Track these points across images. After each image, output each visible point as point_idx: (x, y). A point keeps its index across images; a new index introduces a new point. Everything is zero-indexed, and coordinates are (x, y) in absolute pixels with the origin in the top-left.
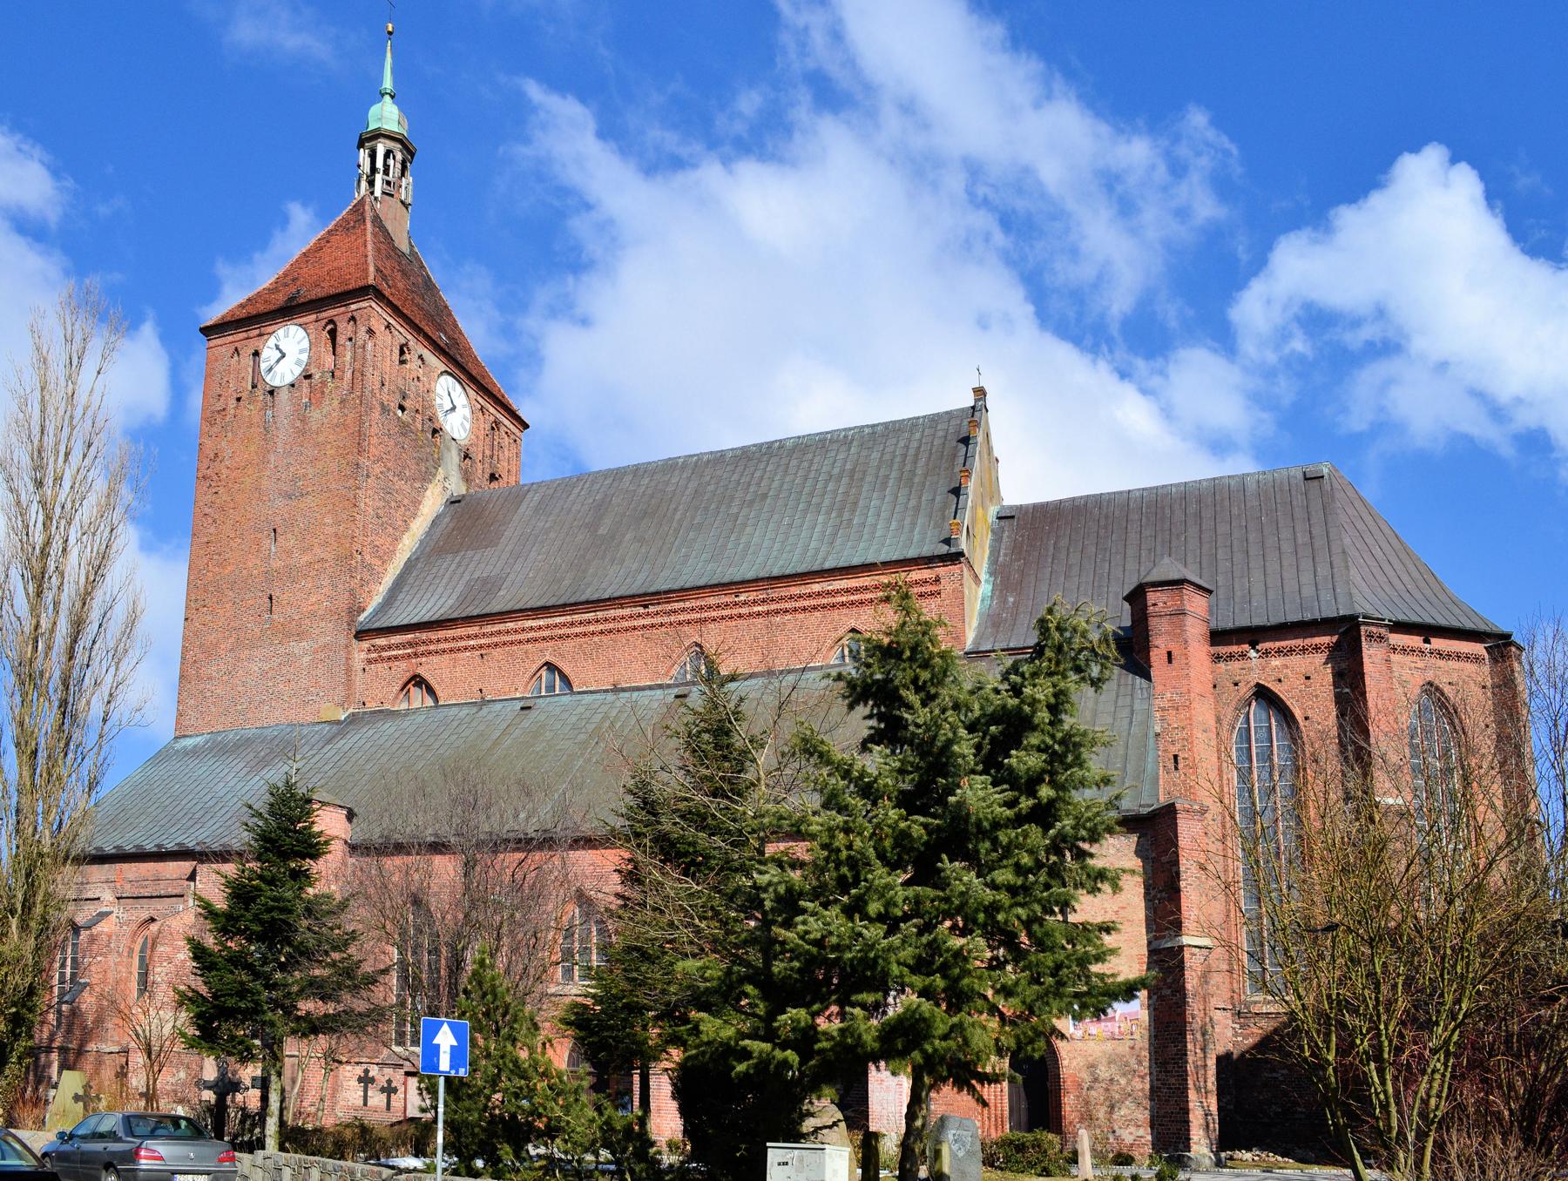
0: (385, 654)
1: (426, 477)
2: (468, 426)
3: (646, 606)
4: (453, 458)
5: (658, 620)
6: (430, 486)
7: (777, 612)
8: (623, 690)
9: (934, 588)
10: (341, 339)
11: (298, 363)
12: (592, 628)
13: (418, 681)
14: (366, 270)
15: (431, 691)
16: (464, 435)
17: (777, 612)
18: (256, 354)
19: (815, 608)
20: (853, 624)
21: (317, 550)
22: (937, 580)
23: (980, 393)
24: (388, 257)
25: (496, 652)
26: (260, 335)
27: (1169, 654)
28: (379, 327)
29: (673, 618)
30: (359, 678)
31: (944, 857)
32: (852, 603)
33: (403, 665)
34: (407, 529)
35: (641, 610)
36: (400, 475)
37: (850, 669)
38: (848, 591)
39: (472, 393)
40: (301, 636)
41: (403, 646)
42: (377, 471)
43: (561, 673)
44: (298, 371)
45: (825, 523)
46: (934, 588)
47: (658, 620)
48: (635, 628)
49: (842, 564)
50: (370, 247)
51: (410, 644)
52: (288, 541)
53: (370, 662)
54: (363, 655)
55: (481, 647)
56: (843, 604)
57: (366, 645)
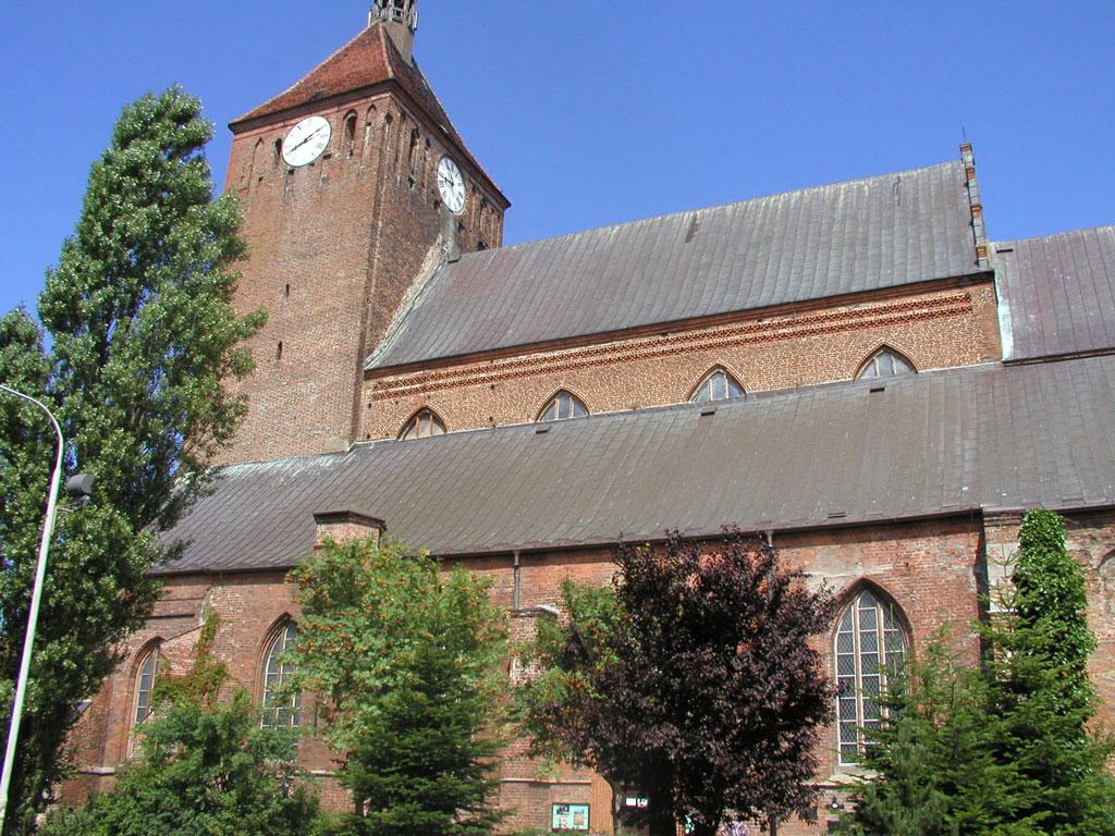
0: (391, 390)
1: (428, 240)
2: (462, 201)
3: (664, 335)
4: (452, 226)
5: (678, 346)
7: (803, 334)
8: (643, 412)
9: (965, 305)
10: (361, 123)
11: (319, 146)
12: (608, 356)
13: (424, 413)
14: (386, 71)
15: (438, 421)
16: (459, 209)
17: (803, 334)
18: (279, 144)
19: (843, 328)
20: (883, 340)
21: (329, 301)
22: (968, 298)
24: (399, 65)
26: (284, 126)
30: (364, 414)
32: (881, 322)
33: (411, 399)
34: (411, 283)
35: (661, 338)
36: (406, 237)
37: (232, 386)
38: (876, 311)
40: (309, 376)
42: (389, 232)
43: (575, 398)
44: (319, 152)
45: (839, 257)
46: (965, 305)
47: (678, 346)
48: (654, 354)
49: (868, 287)
50: (385, 55)
51: (419, 380)
53: (375, 397)
54: (369, 392)
55: (492, 378)
56: (872, 323)
57: (372, 383)
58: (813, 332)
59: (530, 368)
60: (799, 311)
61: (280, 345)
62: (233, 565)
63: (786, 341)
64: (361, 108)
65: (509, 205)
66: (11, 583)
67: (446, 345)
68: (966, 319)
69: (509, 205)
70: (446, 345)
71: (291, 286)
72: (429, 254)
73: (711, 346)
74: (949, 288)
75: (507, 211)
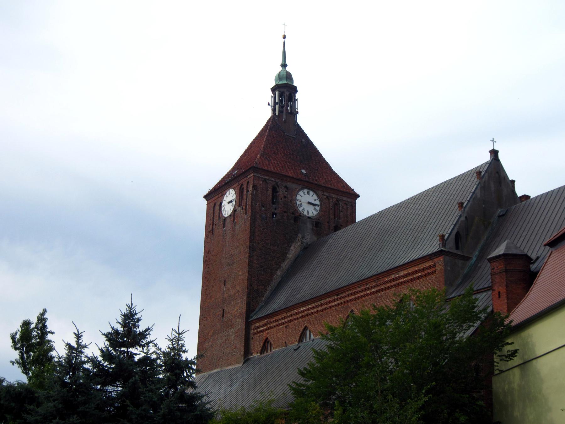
4: (309, 226)
7: (364, 296)
9: (433, 270)
22: (434, 266)
27: (499, 293)
31: (60, 406)
39: (320, 193)
40: (232, 326)
46: (433, 270)
51: (266, 325)
58: (382, 290)
59: (294, 317)
60: (289, 311)
63: (373, 296)
64: (244, 181)
65: (358, 196)
68: (433, 277)
69: (358, 196)
71: (227, 280)
72: (292, 248)
73: (350, 301)
74: (329, 297)
75: (358, 201)
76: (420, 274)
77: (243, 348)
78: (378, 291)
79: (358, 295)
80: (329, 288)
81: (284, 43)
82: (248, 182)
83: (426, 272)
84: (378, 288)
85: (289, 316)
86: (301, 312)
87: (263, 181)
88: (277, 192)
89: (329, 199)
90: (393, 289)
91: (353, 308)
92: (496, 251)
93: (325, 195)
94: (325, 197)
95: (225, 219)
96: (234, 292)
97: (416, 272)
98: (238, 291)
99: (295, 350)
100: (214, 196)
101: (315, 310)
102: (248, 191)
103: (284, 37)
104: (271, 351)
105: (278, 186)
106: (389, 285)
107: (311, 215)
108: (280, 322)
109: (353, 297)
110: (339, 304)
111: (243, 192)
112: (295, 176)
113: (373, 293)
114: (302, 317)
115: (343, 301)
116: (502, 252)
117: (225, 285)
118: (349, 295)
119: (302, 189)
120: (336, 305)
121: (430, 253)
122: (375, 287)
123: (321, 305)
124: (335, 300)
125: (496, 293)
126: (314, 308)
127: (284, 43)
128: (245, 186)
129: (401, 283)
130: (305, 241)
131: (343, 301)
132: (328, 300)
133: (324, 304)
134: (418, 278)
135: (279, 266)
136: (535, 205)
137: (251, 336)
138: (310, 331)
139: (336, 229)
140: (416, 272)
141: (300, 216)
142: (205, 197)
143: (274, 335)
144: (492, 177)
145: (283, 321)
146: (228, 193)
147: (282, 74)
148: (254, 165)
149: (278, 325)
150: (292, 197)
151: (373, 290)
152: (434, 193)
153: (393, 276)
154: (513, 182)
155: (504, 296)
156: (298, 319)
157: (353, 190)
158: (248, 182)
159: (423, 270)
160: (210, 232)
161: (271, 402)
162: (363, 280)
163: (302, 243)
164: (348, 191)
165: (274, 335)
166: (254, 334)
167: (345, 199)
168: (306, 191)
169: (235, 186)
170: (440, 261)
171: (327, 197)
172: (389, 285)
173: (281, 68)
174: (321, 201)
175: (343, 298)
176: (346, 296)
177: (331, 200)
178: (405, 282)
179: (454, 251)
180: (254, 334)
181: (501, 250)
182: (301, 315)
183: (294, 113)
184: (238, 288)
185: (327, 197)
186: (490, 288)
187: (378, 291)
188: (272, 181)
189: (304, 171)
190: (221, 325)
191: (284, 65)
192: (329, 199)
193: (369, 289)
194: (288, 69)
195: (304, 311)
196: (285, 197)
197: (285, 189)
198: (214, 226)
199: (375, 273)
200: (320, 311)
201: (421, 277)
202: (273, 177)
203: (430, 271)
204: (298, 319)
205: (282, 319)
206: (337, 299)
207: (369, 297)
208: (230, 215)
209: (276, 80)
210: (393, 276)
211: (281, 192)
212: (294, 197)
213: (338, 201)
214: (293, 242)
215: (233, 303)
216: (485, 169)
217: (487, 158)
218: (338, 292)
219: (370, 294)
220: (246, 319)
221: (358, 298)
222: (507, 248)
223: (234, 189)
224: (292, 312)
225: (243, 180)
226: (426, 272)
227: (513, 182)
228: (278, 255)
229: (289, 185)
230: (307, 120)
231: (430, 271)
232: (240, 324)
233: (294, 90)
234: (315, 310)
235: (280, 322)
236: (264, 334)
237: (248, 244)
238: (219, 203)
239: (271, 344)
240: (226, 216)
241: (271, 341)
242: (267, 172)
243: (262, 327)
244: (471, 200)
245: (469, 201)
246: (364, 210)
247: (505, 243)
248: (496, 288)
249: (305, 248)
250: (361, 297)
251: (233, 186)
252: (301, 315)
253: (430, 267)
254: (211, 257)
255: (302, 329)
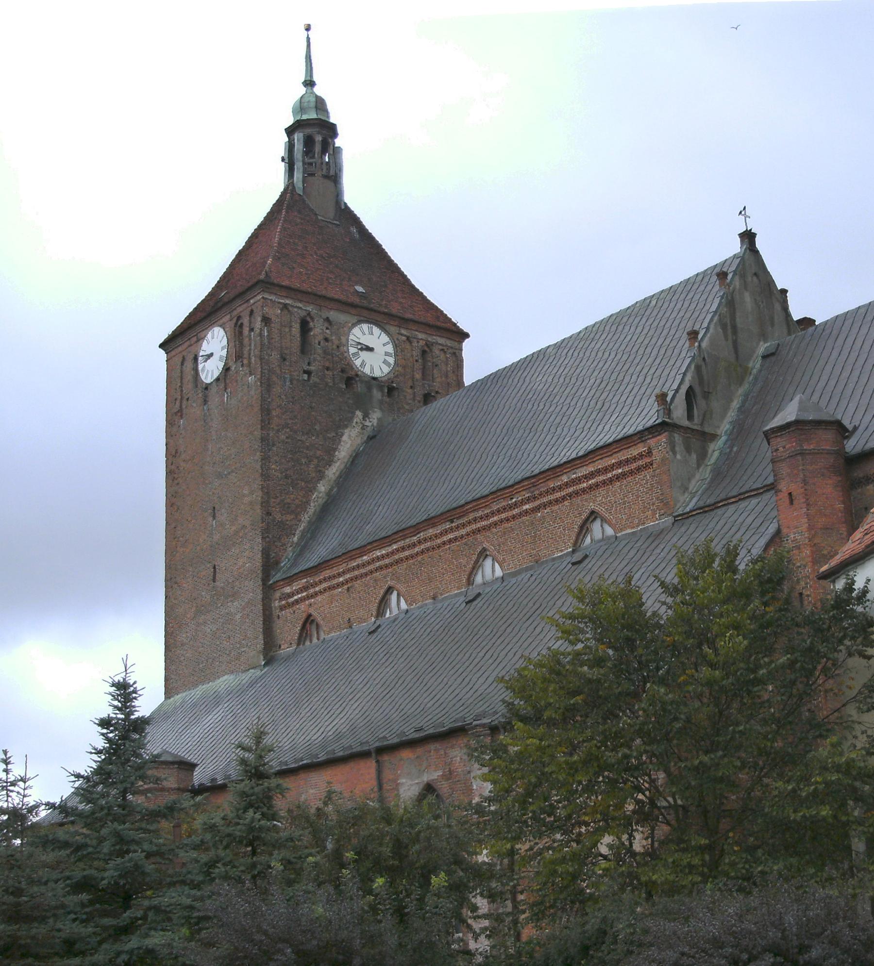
2: (391, 360)
6: (347, 432)
7: (507, 520)
9: (648, 460)
22: (649, 453)
23: (748, 237)
25: (357, 584)
27: (790, 494)
28: (274, 313)
29: (610, 475)
35: (448, 525)
39: (393, 329)
40: (235, 596)
41: (619, 464)
46: (648, 460)
51: (305, 588)
52: (223, 516)
58: (545, 506)
59: (363, 571)
60: (353, 558)
61: (214, 568)
62: (352, 764)
64: (241, 309)
65: (466, 336)
66: (416, 840)
67: (646, 419)
68: (647, 474)
69: (466, 336)
70: (646, 419)
71: (217, 507)
72: (345, 438)
74: (434, 525)
75: (466, 344)
76: (620, 471)
77: (261, 637)
78: (537, 509)
79: (495, 518)
80: (434, 508)
81: (308, 39)
82: (252, 312)
83: (634, 466)
84: (537, 503)
85: (354, 569)
86: (378, 559)
87: (282, 310)
88: (310, 330)
89: (411, 342)
90: (566, 503)
91: (486, 545)
92: (776, 419)
93: (402, 335)
94: (404, 338)
95: (207, 387)
96: (234, 528)
97: (613, 467)
98: (244, 527)
99: (370, 633)
100: (181, 342)
101: (407, 553)
102: (252, 330)
103: (308, 28)
104: (318, 639)
105: (312, 319)
106: (558, 495)
107: (377, 374)
108: (335, 581)
109: (484, 523)
110: (456, 539)
111: (241, 333)
112: (343, 298)
113: (526, 512)
114: (381, 568)
115: (463, 532)
116: (792, 418)
117: (214, 517)
118: (330, 578)
119: (360, 322)
120: (450, 541)
121: (640, 428)
122: (528, 500)
123: (364, 565)
124: (446, 532)
125: (784, 495)
126: (403, 549)
127: (308, 39)
128: (245, 321)
129: (584, 491)
130: (370, 424)
131: (463, 532)
132: (431, 532)
133: (425, 540)
134: (618, 478)
135: (321, 476)
136: (835, 332)
137: (276, 612)
138: (398, 595)
139: (427, 399)
140: (613, 467)
141: (357, 375)
142: (162, 346)
143: (322, 606)
144: (746, 281)
145: (341, 579)
146: (209, 335)
147: (306, 99)
148: (262, 277)
149: (330, 588)
150: (340, 339)
151: (527, 507)
152: (631, 320)
153: (565, 478)
154: (784, 292)
155: (800, 500)
156: (371, 572)
157: (455, 325)
158: (252, 312)
159: (627, 461)
160: (176, 413)
161: (339, 736)
162: (504, 488)
163: (364, 427)
164: (448, 325)
165: (322, 606)
166: (282, 608)
167: (441, 341)
168: (365, 327)
169: (225, 320)
170: (659, 444)
171: (408, 338)
172: (558, 495)
173: (303, 90)
174: (396, 346)
175: (464, 525)
176: (469, 523)
177: (415, 344)
178: (590, 488)
179: (686, 423)
180: (282, 608)
181: (789, 413)
182: (378, 564)
183: (334, 177)
184: (241, 520)
185: (408, 338)
186: (771, 487)
187: (537, 509)
188: (300, 308)
189: (360, 289)
190: (212, 597)
191: (309, 83)
192: (411, 342)
193: (516, 505)
194: (317, 90)
195: (383, 557)
196: (326, 340)
197: (326, 325)
198: (185, 402)
199: (528, 475)
200: (417, 554)
201: (624, 475)
202: (301, 301)
203: (640, 463)
204: (371, 572)
205: (339, 575)
206: (451, 530)
207: (517, 522)
208: (218, 379)
209: (294, 112)
210: (565, 478)
211: (318, 329)
212: (343, 339)
213: (429, 345)
214: (346, 427)
215: (235, 550)
216: (733, 268)
217: (735, 247)
218: (452, 514)
219: (520, 515)
220: (263, 580)
221: (495, 524)
222: (802, 408)
223: (222, 326)
224: (359, 561)
225: (239, 309)
226: (634, 466)
227: (784, 292)
228: (319, 453)
229: (333, 315)
230: (360, 193)
231: (640, 463)
232: (252, 590)
233: (331, 130)
234: (407, 553)
235: (335, 581)
236: (302, 606)
237: (258, 433)
238: (192, 356)
239: (318, 626)
240: (208, 381)
241: (319, 619)
242: (289, 290)
243: (298, 593)
244: (712, 326)
245: (708, 328)
246: (478, 362)
247: (797, 399)
248: (783, 486)
249: (371, 438)
250: (501, 521)
251: (221, 322)
252: (378, 564)
253: (641, 456)
254: (182, 464)
255: (382, 592)
